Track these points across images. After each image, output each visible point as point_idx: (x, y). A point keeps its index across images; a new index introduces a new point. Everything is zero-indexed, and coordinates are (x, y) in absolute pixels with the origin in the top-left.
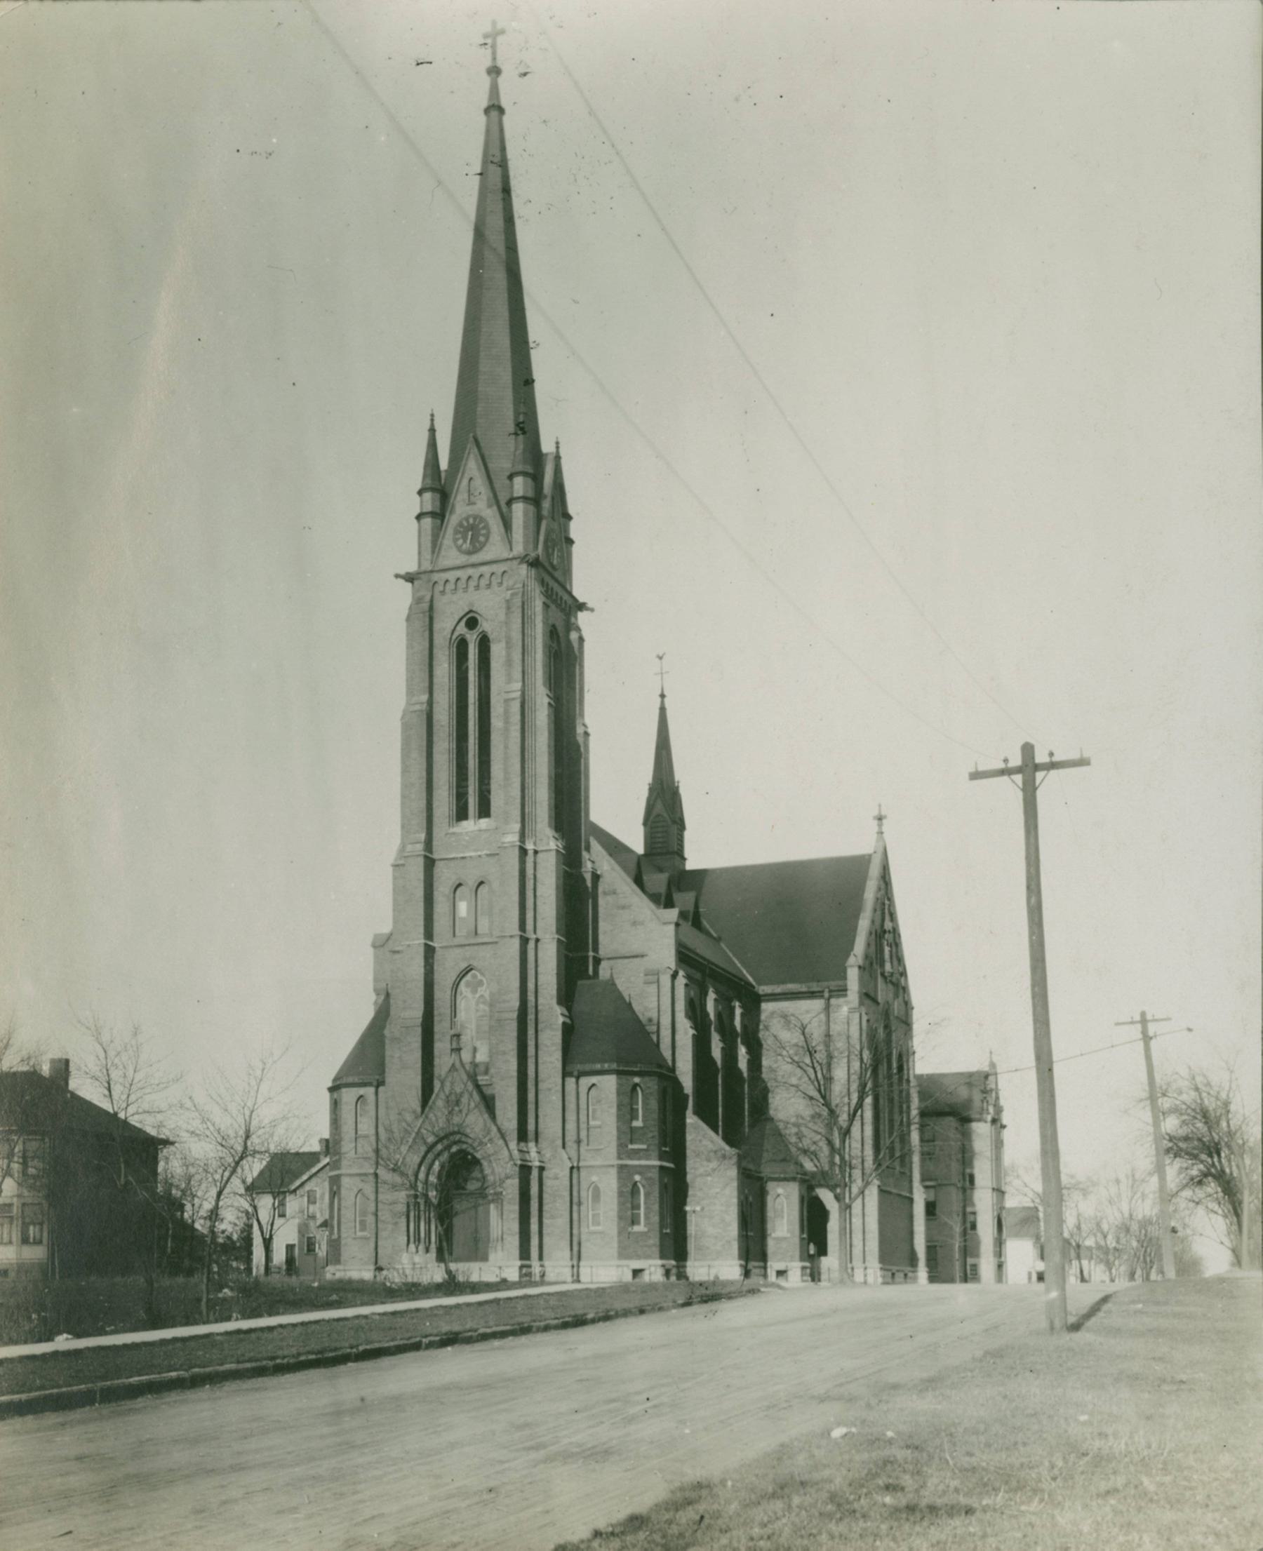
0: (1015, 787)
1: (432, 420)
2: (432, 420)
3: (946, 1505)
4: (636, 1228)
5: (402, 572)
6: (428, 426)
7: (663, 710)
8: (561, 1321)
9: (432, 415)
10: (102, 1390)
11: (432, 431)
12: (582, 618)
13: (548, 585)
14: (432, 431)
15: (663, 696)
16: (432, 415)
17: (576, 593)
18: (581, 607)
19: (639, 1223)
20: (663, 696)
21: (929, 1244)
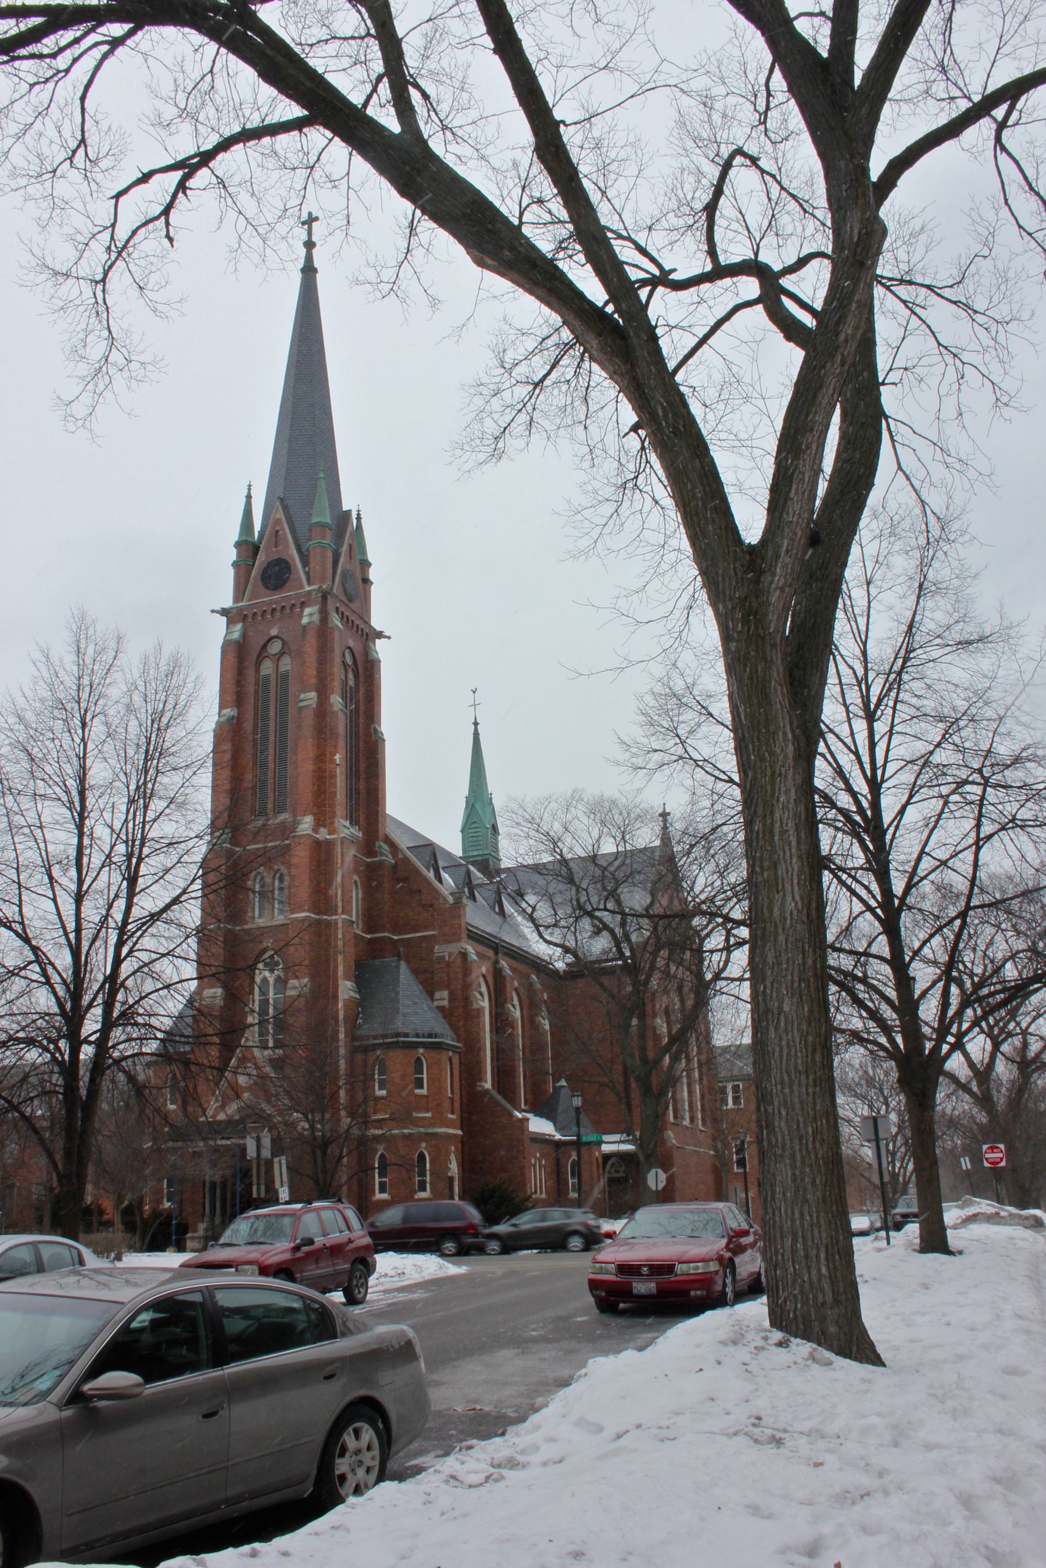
0: (630, 261)
1: (249, 489)
2: (249, 489)
3: (358, 1491)
4: (418, 1091)
5: (218, 608)
6: (246, 493)
7: (476, 735)
8: (1026, 1212)
9: (250, 486)
10: (422, 1079)
11: (249, 497)
12: (380, 645)
13: (342, 613)
14: (249, 497)
15: (476, 724)
16: (250, 486)
17: (373, 624)
18: (380, 635)
19: (422, 1087)
20: (476, 724)
21: (47, 1220)
